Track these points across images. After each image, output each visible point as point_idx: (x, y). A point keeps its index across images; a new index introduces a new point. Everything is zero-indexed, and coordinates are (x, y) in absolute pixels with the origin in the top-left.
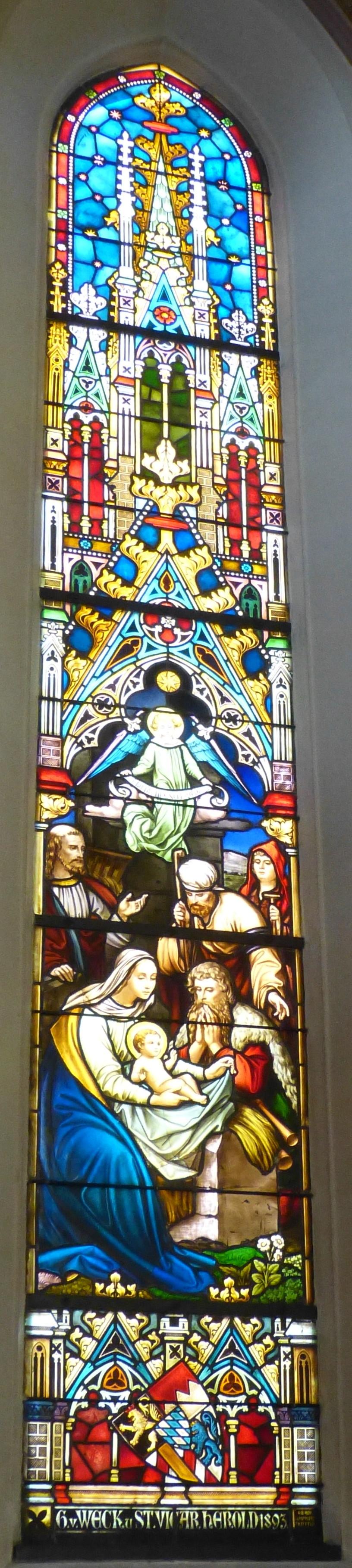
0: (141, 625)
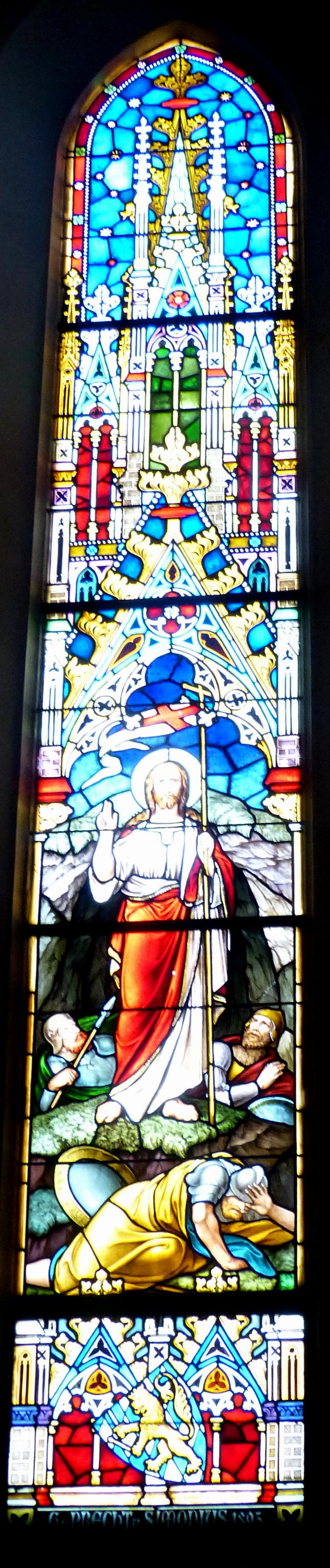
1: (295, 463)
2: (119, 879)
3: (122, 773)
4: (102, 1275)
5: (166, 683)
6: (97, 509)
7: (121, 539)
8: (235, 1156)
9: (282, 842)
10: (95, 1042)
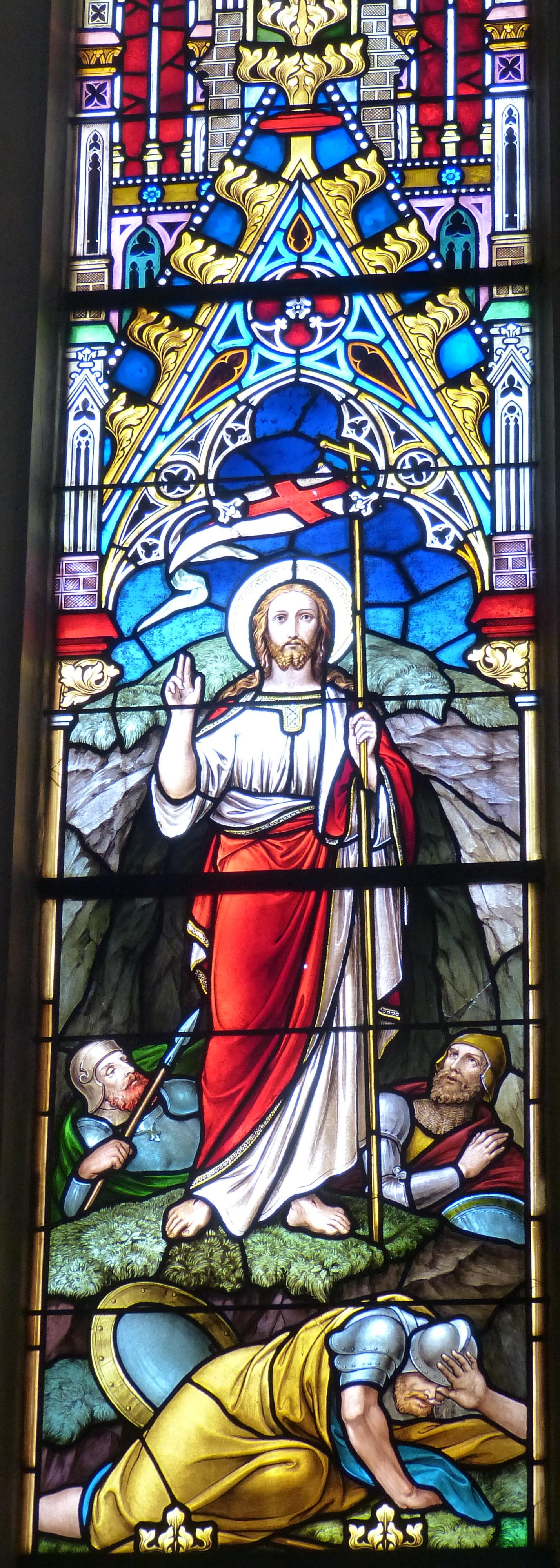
0: (248, 324)
1: (524, 27)
2: (205, 796)
3: (208, 603)
4: (175, 1516)
5: (287, 440)
6: (161, 116)
7: (205, 172)
8: (417, 1302)
9: (502, 728)
10: (163, 1092)
